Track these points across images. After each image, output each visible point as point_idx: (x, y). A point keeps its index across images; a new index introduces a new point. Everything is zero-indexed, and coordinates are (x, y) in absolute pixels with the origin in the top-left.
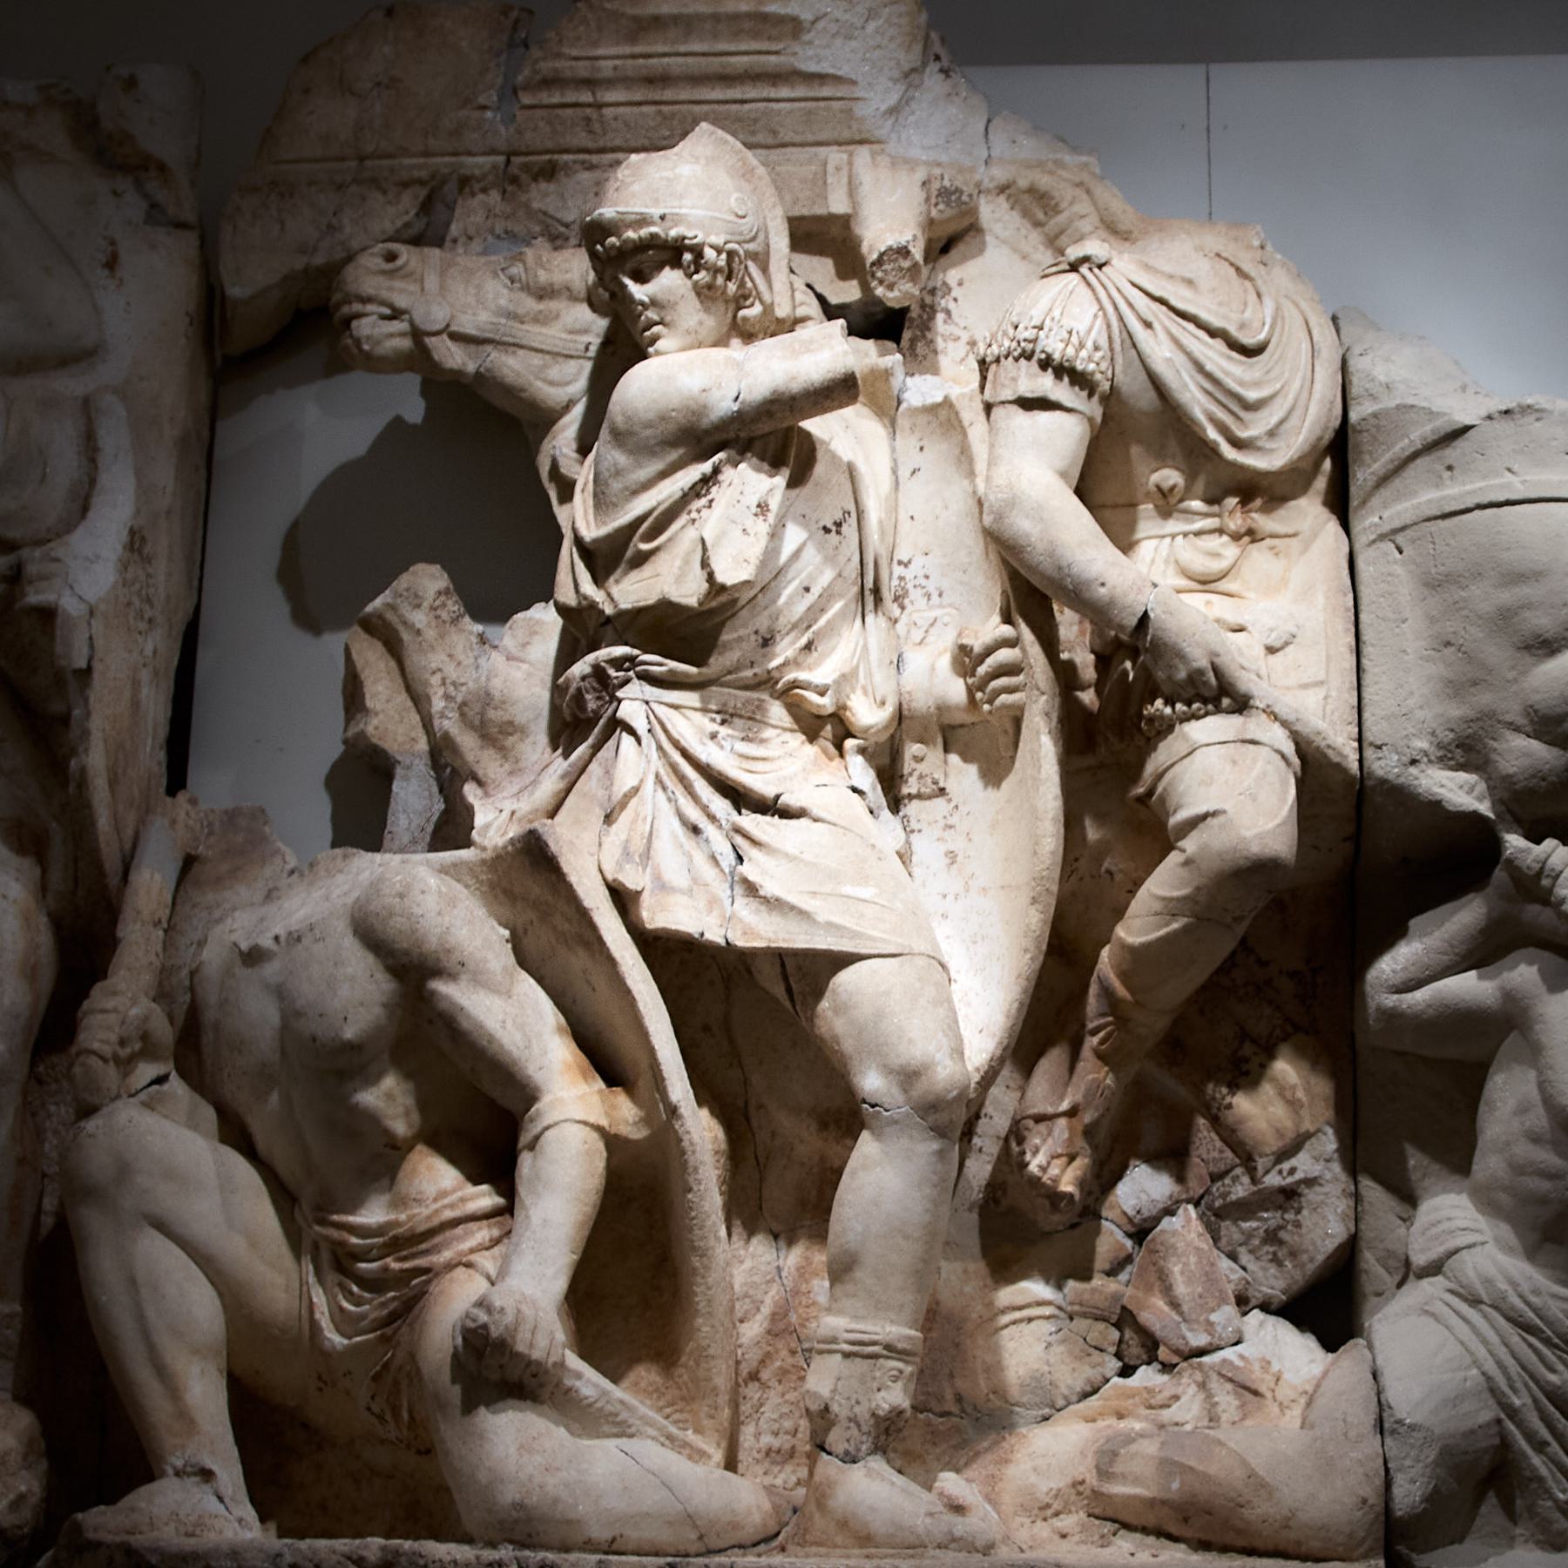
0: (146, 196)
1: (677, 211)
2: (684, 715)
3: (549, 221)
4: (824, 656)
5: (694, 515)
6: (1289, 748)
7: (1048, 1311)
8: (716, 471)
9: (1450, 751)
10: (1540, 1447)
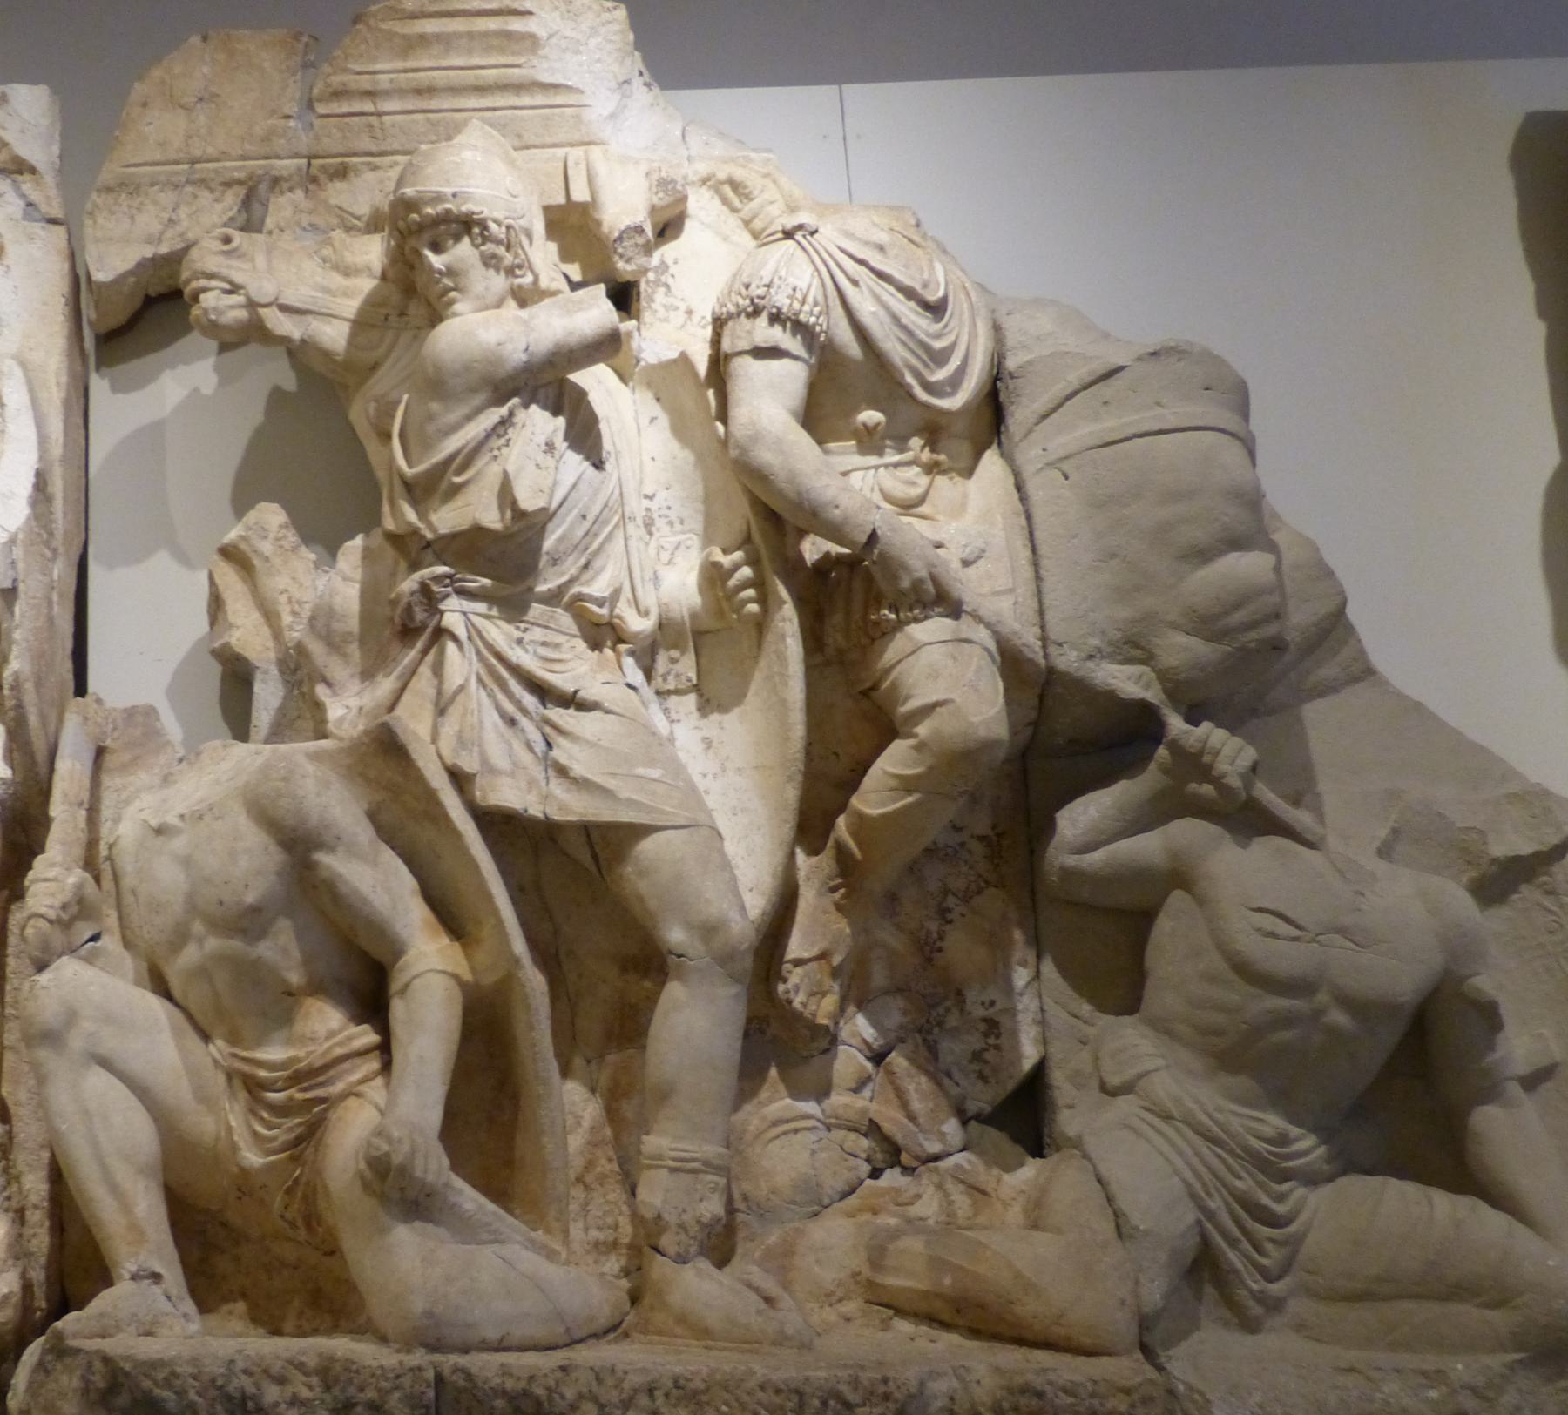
0: (23, 196)
2: (494, 624)
3: (346, 216)
4: (598, 573)
5: (496, 452)
6: (992, 646)
7: (811, 1123)
8: (511, 414)
9: (1118, 647)
10: (1233, 1243)
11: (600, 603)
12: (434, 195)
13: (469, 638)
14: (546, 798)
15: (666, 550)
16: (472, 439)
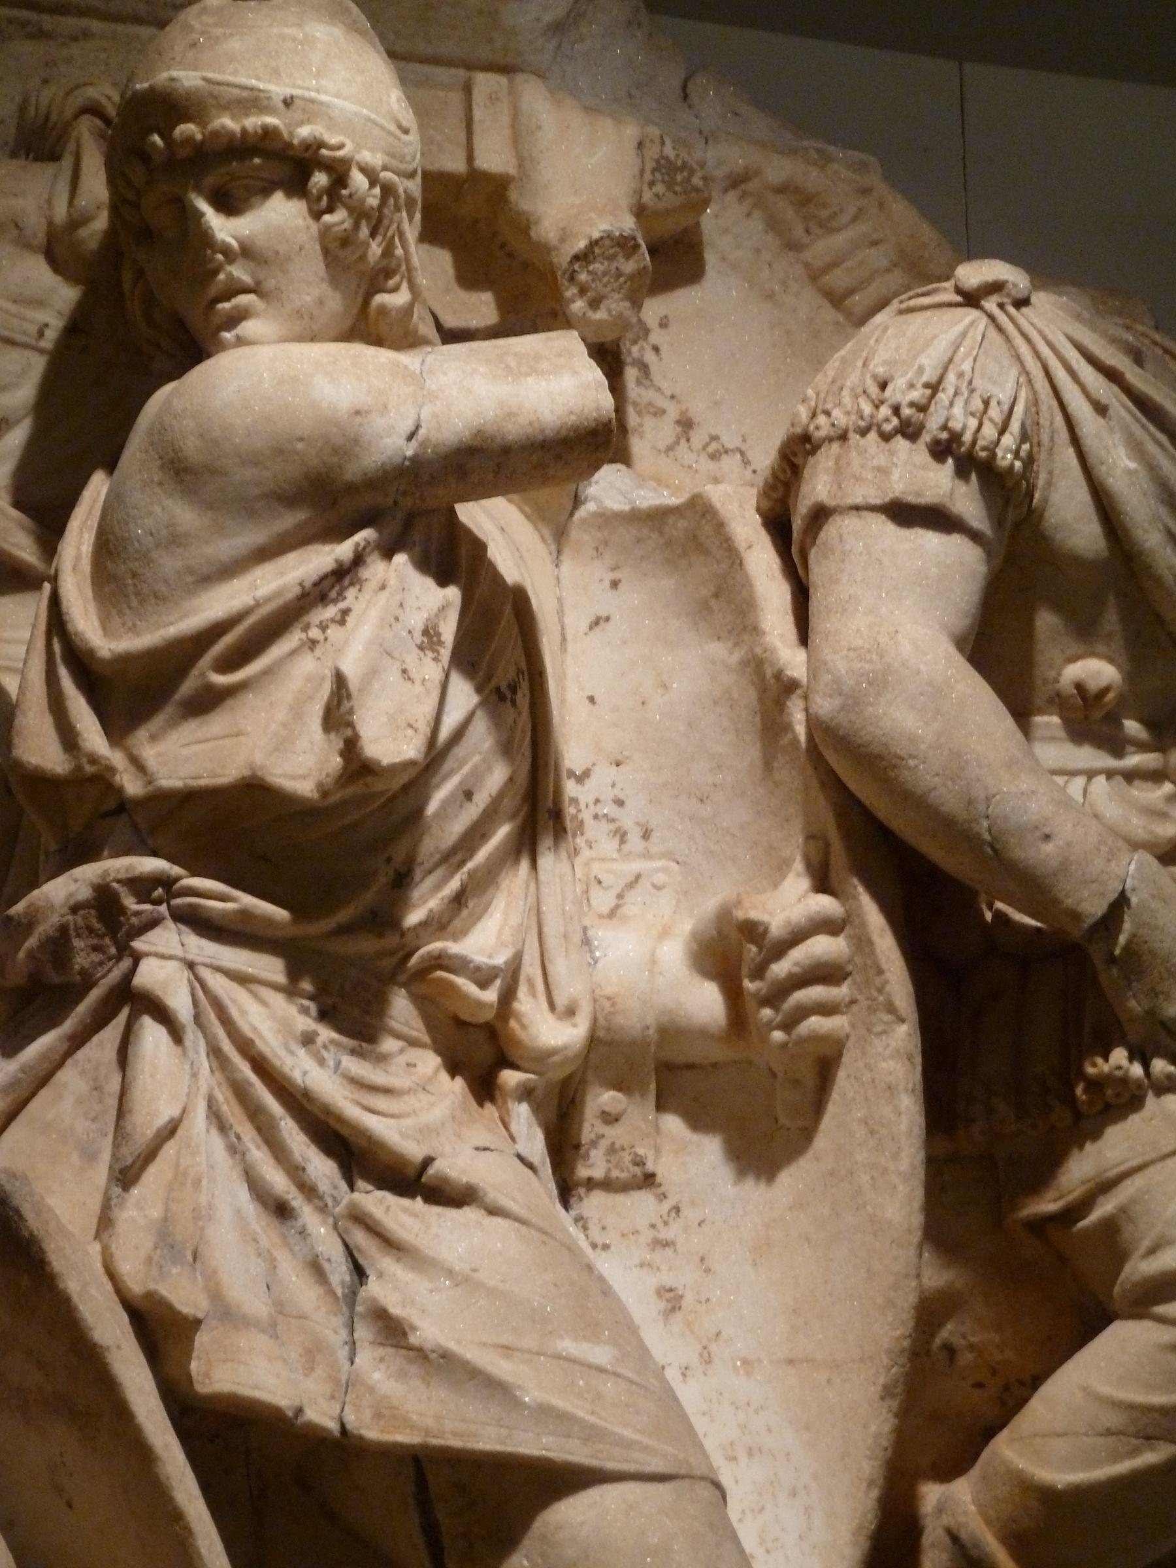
1: (313, 94)
4: (477, 917)
5: (314, 633)
8: (358, 560)
11: (483, 978)
12: (245, 94)
13: (197, 1018)
14: (347, 1387)
15: (607, 888)
16: (268, 599)
